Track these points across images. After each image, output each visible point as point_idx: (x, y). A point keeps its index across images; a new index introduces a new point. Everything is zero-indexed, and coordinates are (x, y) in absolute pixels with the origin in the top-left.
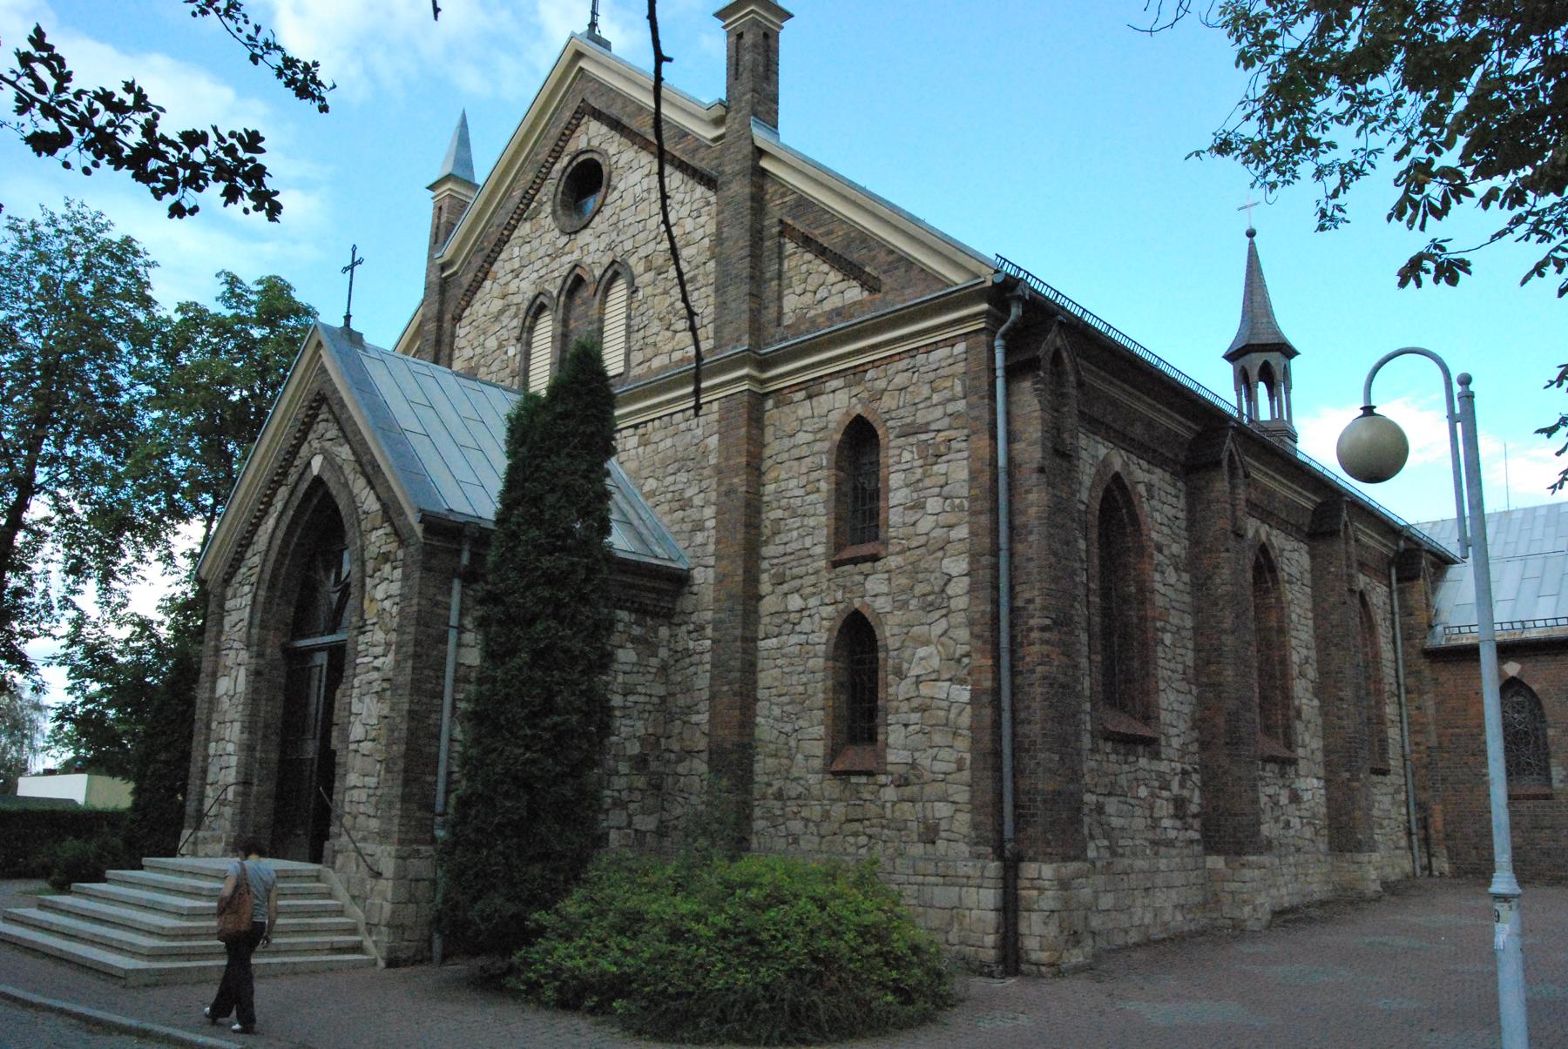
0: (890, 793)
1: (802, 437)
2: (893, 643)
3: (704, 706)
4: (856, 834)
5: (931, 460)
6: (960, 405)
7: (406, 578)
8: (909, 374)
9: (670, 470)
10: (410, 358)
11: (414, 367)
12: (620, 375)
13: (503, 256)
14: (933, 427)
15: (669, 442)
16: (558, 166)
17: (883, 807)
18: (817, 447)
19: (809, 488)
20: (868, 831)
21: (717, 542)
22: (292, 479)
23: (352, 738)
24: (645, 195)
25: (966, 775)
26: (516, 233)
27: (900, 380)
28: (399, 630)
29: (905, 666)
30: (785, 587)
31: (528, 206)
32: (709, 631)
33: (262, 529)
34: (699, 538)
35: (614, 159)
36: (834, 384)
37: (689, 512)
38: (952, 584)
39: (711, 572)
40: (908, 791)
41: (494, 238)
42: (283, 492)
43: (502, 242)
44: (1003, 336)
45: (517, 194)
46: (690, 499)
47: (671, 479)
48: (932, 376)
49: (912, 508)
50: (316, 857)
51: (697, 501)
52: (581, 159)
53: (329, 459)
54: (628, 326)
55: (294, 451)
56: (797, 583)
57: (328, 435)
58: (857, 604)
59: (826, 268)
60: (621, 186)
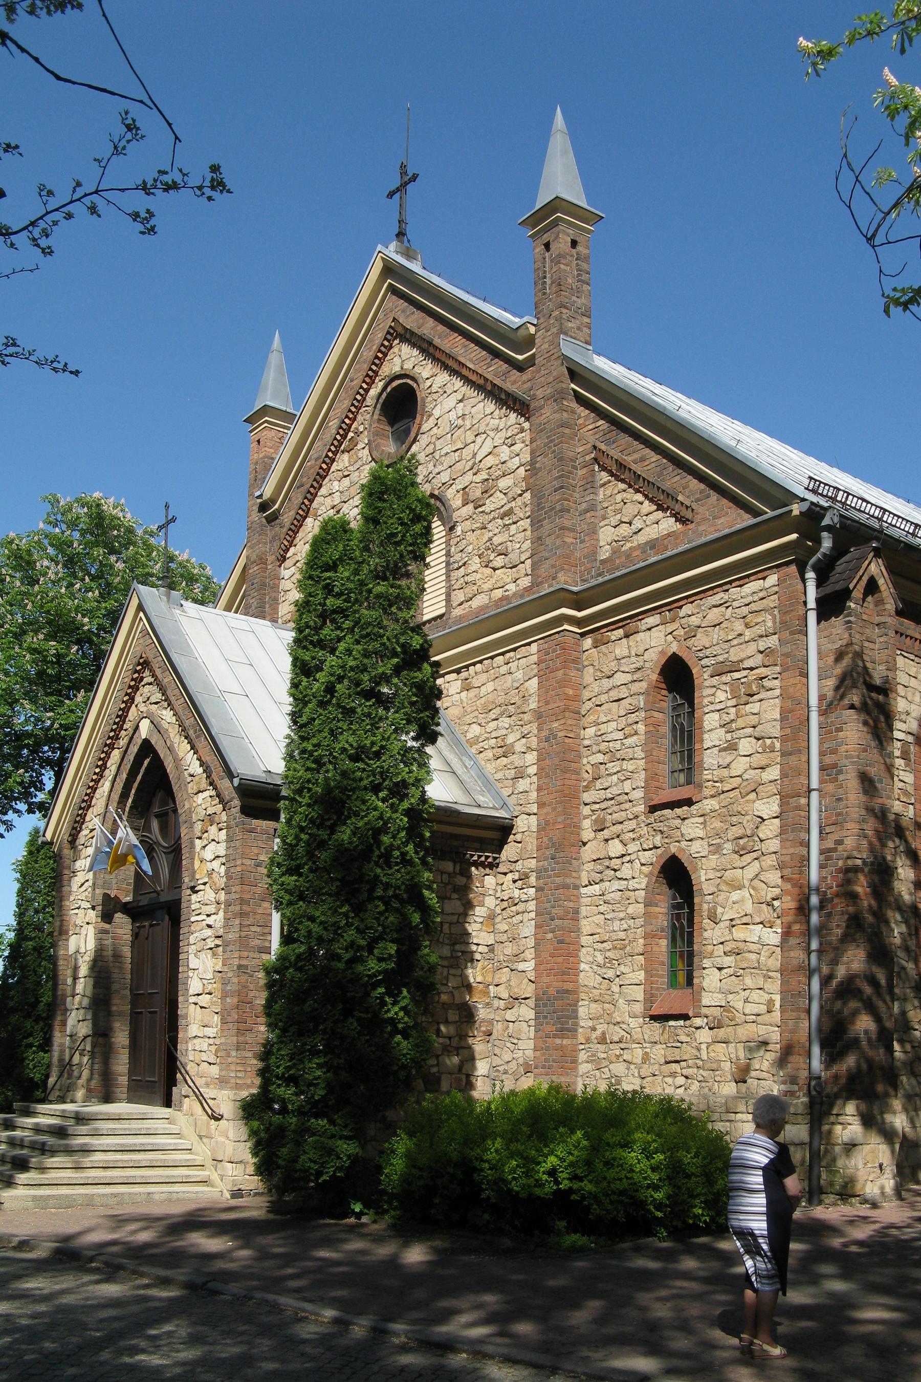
0: (705, 1036)
1: (620, 678)
2: (707, 888)
3: (530, 954)
4: (673, 1075)
5: (744, 699)
6: (773, 641)
7: (229, 839)
8: (722, 609)
9: (492, 716)
10: (232, 614)
11: (234, 623)
12: (441, 616)
13: (323, 491)
14: (747, 664)
15: (490, 686)
16: (373, 392)
17: (699, 1050)
18: (636, 687)
19: (627, 731)
20: (685, 1072)
21: (539, 789)
22: (122, 743)
23: (191, 992)
24: (460, 422)
25: (777, 1015)
26: (334, 467)
27: (714, 615)
28: (226, 889)
29: (719, 910)
30: (606, 833)
31: (344, 437)
32: (533, 880)
33: (98, 794)
34: (522, 784)
35: (428, 383)
36: (651, 620)
37: (512, 758)
38: (762, 827)
39: (534, 818)
40: (721, 1033)
41: (312, 473)
42: (116, 755)
43: (321, 476)
44: (815, 569)
45: (334, 424)
46: (512, 745)
47: (493, 725)
48: (745, 610)
49: (725, 749)
50: (168, 1103)
51: (519, 747)
52: (395, 384)
53: (156, 726)
54: (448, 564)
55: (122, 716)
56: (618, 828)
57: (153, 700)
58: (673, 849)
59: (640, 497)
60: (437, 413)
